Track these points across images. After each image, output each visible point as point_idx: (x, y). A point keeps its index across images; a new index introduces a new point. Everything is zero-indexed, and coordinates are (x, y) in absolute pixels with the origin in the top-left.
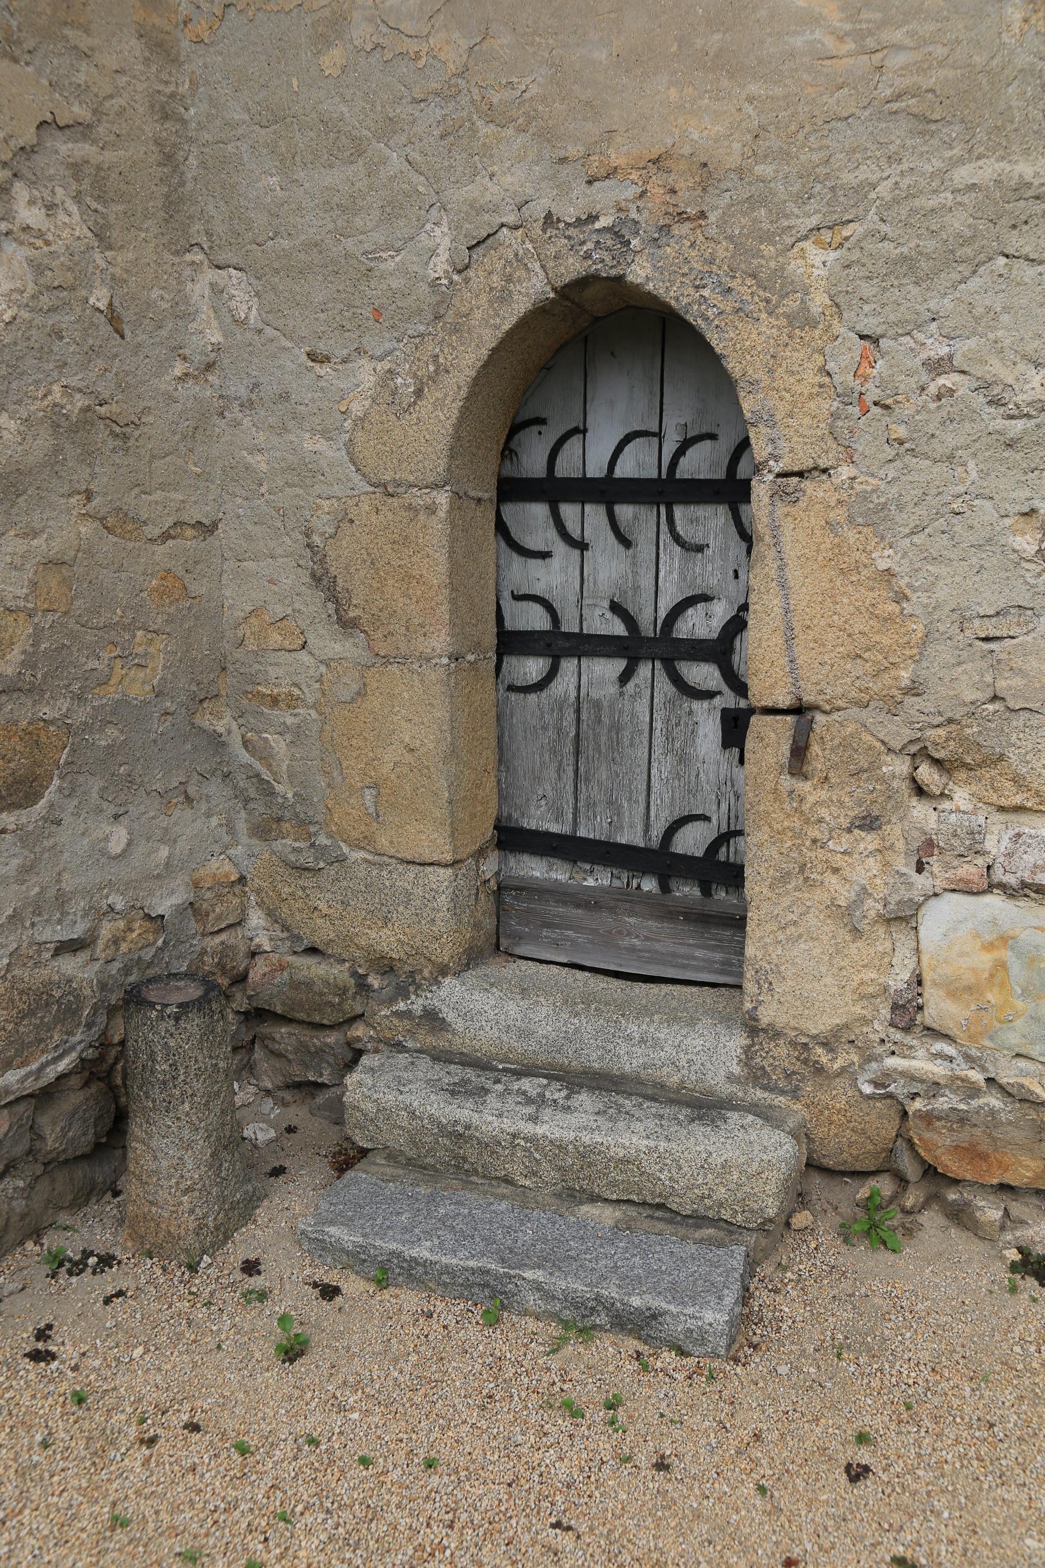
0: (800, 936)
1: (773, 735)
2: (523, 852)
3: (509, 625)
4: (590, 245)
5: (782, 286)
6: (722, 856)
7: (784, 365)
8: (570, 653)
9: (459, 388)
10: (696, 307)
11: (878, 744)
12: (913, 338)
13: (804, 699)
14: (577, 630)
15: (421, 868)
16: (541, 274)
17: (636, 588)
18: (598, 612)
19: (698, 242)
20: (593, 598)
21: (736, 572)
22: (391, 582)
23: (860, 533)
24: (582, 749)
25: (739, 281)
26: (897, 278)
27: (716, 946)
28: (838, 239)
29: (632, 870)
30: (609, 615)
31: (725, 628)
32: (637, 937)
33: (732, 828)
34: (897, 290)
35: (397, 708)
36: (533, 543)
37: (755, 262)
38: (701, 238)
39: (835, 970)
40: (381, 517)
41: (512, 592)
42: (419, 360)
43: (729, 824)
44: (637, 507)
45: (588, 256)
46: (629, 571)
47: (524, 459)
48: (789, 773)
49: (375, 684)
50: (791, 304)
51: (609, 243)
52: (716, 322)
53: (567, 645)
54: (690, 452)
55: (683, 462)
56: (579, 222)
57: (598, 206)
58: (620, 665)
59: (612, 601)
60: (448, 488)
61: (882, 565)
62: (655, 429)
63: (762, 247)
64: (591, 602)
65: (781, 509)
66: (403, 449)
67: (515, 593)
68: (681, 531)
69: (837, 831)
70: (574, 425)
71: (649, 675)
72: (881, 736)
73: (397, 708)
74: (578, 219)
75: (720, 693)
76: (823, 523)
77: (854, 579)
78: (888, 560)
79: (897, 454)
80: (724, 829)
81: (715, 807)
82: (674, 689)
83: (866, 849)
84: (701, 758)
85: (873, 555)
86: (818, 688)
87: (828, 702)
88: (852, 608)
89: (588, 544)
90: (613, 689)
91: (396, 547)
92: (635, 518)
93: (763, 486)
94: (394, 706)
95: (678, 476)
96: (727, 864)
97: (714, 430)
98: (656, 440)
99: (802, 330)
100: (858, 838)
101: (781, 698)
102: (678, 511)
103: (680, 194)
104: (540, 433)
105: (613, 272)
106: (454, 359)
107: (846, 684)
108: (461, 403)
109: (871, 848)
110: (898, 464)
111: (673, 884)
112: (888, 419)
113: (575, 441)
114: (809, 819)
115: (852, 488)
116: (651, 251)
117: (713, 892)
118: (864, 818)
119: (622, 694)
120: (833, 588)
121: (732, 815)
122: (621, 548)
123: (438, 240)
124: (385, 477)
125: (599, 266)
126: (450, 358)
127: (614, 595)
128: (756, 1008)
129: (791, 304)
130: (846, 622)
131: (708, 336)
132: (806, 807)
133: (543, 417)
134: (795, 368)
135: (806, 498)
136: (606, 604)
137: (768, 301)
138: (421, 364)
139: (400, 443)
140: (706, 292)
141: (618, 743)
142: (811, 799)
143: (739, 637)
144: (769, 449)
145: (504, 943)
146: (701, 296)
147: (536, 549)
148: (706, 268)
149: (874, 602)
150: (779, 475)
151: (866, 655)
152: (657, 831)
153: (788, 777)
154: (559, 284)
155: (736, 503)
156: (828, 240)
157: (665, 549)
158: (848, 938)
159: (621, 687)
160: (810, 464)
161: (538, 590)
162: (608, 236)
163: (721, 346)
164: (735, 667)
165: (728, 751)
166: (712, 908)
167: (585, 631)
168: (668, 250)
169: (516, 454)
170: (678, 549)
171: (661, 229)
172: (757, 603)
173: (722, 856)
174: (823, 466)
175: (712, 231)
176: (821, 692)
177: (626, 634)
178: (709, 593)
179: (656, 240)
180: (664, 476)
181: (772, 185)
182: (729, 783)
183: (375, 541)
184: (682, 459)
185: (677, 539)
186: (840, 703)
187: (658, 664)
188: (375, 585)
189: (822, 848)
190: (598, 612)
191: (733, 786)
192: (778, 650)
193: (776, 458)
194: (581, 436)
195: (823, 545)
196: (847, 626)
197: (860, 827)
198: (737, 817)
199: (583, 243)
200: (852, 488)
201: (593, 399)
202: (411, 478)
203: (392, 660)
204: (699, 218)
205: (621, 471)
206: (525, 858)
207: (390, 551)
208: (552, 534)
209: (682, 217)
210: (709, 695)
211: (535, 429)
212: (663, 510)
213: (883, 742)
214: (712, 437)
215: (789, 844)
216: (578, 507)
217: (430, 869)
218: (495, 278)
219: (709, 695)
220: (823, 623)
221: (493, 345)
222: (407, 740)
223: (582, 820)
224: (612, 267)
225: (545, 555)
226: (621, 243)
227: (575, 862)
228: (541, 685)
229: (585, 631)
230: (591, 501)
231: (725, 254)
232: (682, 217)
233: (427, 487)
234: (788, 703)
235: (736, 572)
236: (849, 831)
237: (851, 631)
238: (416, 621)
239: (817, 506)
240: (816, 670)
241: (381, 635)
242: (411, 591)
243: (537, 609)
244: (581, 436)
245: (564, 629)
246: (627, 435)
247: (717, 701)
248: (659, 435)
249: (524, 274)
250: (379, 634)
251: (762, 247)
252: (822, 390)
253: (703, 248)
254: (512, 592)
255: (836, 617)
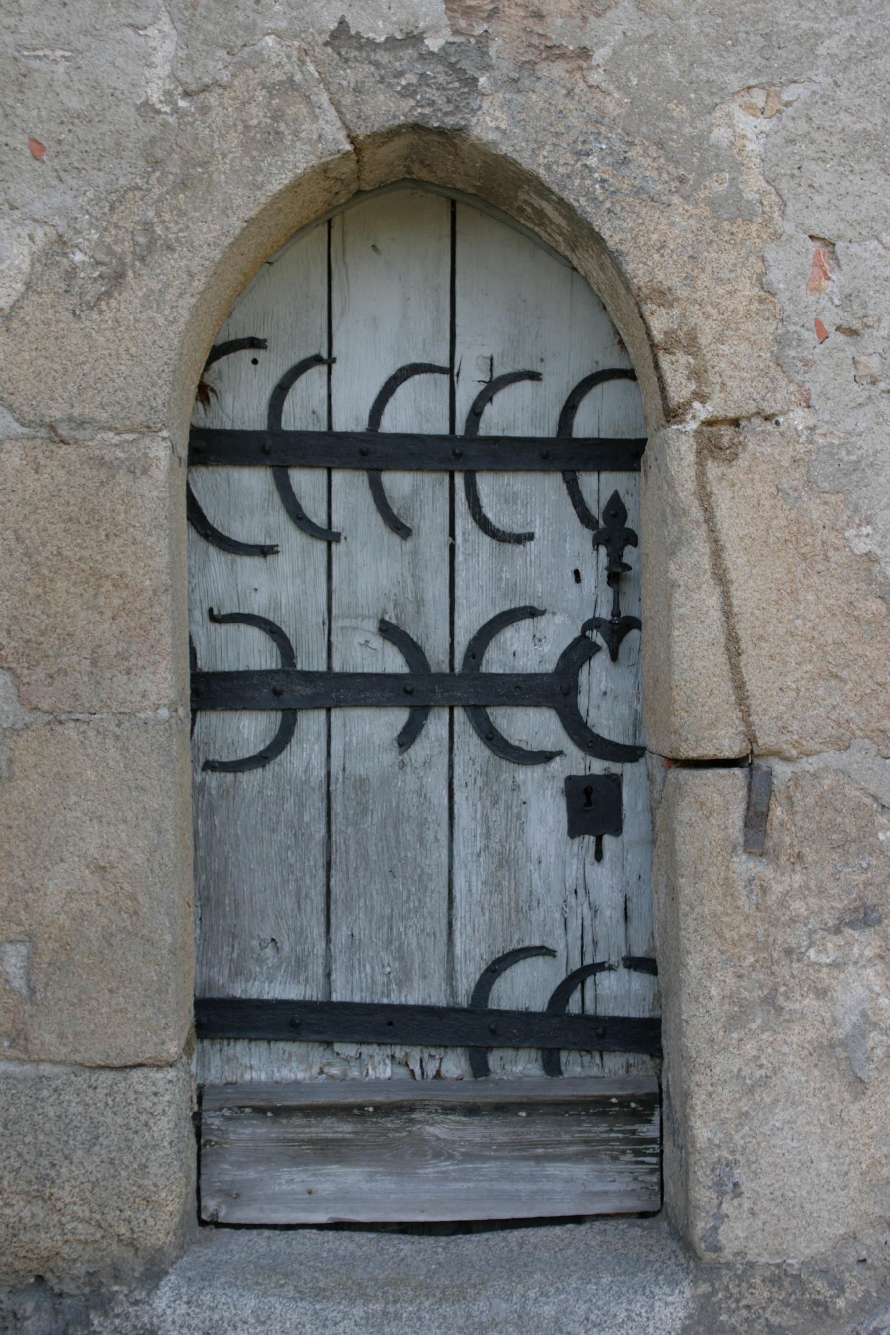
0: (776, 1101)
1: (717, 798)
2: (237, 1039)
3: (204, 665)
4: (411, 78)
5: (702, 160)
6: (574, 1006)
7: (708, 270)
8: (313, 704)
9: (191, 275)
10: (577, 182)
11: (868, 801)
12: (880, 242)
13: (761, 742)
14: (323, 668)
15: (119, 1076)
16: (332, 114)
17: (419, 603)
18: (359, 638)
19: (577, 91)
20: (348, 616)
21: (577, 573)
22: (61, 585)
23: (825, 503)
24: (336, 858)
25: (639, 149)
26: (858, 161)
27: (577, 1154)
28: (774, 105)
29: (427, 1046)
30: (377, 642)
31: (565, 655)
32: (451, 1157)
33: (588, 961)
34: (858, 178)
35: (73, 799)
36: (240, 532)
37: (662, 125)
38: (582, 85)
39: (831, 1149)
40: (46, 478)
41: (211, 610)
42: (116, 226)
43: (583, 954)
44: (419, 476)
45: (408, 92)
46: (408, 575)
47: (228, 400)
48: (745, 851)
49: (31, 760)
50: (717, 186)
51: (441, 79)
52: (608, 204)
53: (309, 691)
54: (501, 397)
55: (489, 411)
56: (391, 43)
57: (422, 24)
58: (399, 717)
59: (382, 621)
60: (165, 433)
61: (861, 547)
62: (445, 363)
63: (671, 106)
64: (345, 623)
65: (713, 469)
66: (86, 368)
67: (215, 612)
68: (489, 512)
69: (821, 932)
70: (313, 352)
71: (445, 733)
72: (872, 788)
73: (73, 799)
74: (391, 39)
75: (560, 753)
76: (773, 490)
77: (820, 567)
78: (868, 541)
79: (870, 397)
80: (576, 965)
81: (560, 931)
82: (487, 752)
83: (861, 955)
84: (534, 856)
85: (847, 534)
86: (780, 724)
87: (795, 744)
88: (821, 608)
89: (338, 535)
90: (390, 757)
91: (73, 527)
92: (416, 492)
93: (684, 437)
94: (67, 795)
95: (482, 432)
96: (583, 1017)
97: (536, 367)
98: (446, 378)
99: (732, 224)
100: (851, 940)
101: (726, 742)
102: (486, 483)
103: (549, 20)
104: (255, 362)
105: (450, 121)
106: (181, 230)
107: (818, 716)
108: (193, 301)
109: (868, 953)
110: (869, 410)
111: (494, 1060)
112: (853, 349)
113: (317, 374)
114: (778, 920)
115: (811, 442)
116: (508, 96)
117: (563, 1068)
118: (856, 910)
119: (403, 765)
120: (792, 581)
121: (588, 939)
122: (395, 539)
123: (153, 44)
124: (52, 412)
125: (427, 111)
126: (175, 229)
127: (385, 611)
128: (715, 1229)
129: (717, 186)
130: (814, 629)
131: (597, 224)
132: (772, 899)
133: (260, 336)
134: (725, 275)
135: (747, 456)
136: (372, 625)
137: (682, 180)
138: (121, 234)
139: (81, 359)
140: (593, 161)
141: (398, 843)
142: (778, 889)
143: (586, 667)
144: (693, 386)
145: (210, 1204)
146: (586, 166)
147: (251, 542)
148: (591, 128)
149: (852, 598)
150: (709, 423)
151: (844, 674)
152: (466, 985)
153: (744, 857)
154: (362, 132)
155: (574, 472)
156: (761, 104)
157: (465, 541)
158: (846, 1095)
159: (401, 753)
160: (752, 408)
161: (257, 605)
162: (440, 68)
163: (616, 238)
164: (583, 713)
165: (577, 840)
166: (559, 1090)
167: (337, 668)
168: (534, 98)
169: (213, 390)
170: (487, 540)
171: (522, 66)
172: (683, 605)
173: (574, 1006)
174: (769, 411)
175: (596, 77)
176: (783, 729)
177: (406, 670)
178: (536, 605)
179: (516, 81)
180: (460, 430)
181: (682, 22)
182: (581, 892)
183: (32, 518)
184: (488, 408)
185: (484, 525)
186: (812, 745)
187: (459, 713)
188: (32, 591)
189: (799, 960)
190: (359, 638)
191: (587, 893)
192: (718, 672)
193: (702, 398)
194: (324, 368)
195: (775, 522)
196: (816, 634)
197: (852, 924)
198: (595, 943)
199: (400, 74)
200: (811, 442)
201: (342, 314)
202: (103, 416)
203: (63, 717)
204: (579, 57)
205: (390, 424)
206: (239, 1049)
207: (61, 534)
208: (280, 518)
209: (554, 53)
210: (546, 757)
211: (247, 355)
212: (459, 479)
213: (875, 798)
214: (534, 376)
215: (751, 959)
216: (322, 474)
217: (137, 1075)
218: (253, 109)
219: (546, 757)
220: (781, 631)
221: (252, 213)
222: (93, 851)
223: (338, 977)
224: (446, 114)
225: (265, 551)
226: (460, 80)
227: (329, 1044)
228: (262, 759)
229: (337, 668)
230: (340, 467)
231: (618, 111)
232: (554, 53)
233: (132, 431)
234: (736, 749)
235: (577, 573)
236: (837, 931)
237: (822, 641)
238: (112, 649)
239: (764, 467)
240: (777, 699)
241: (42, 676)
242: (101, 601)
243: (254, 636)
244: (324, 368)
245: (302, 665)
246: (401, 370)
247: (559, 769)
248: (450, 371)
249: (304, 110)
250: (40, 674)
251: (671, 106)
252: (763, 307)
253: (584, 99)
254: (211, 610)
255: (799, 622)
